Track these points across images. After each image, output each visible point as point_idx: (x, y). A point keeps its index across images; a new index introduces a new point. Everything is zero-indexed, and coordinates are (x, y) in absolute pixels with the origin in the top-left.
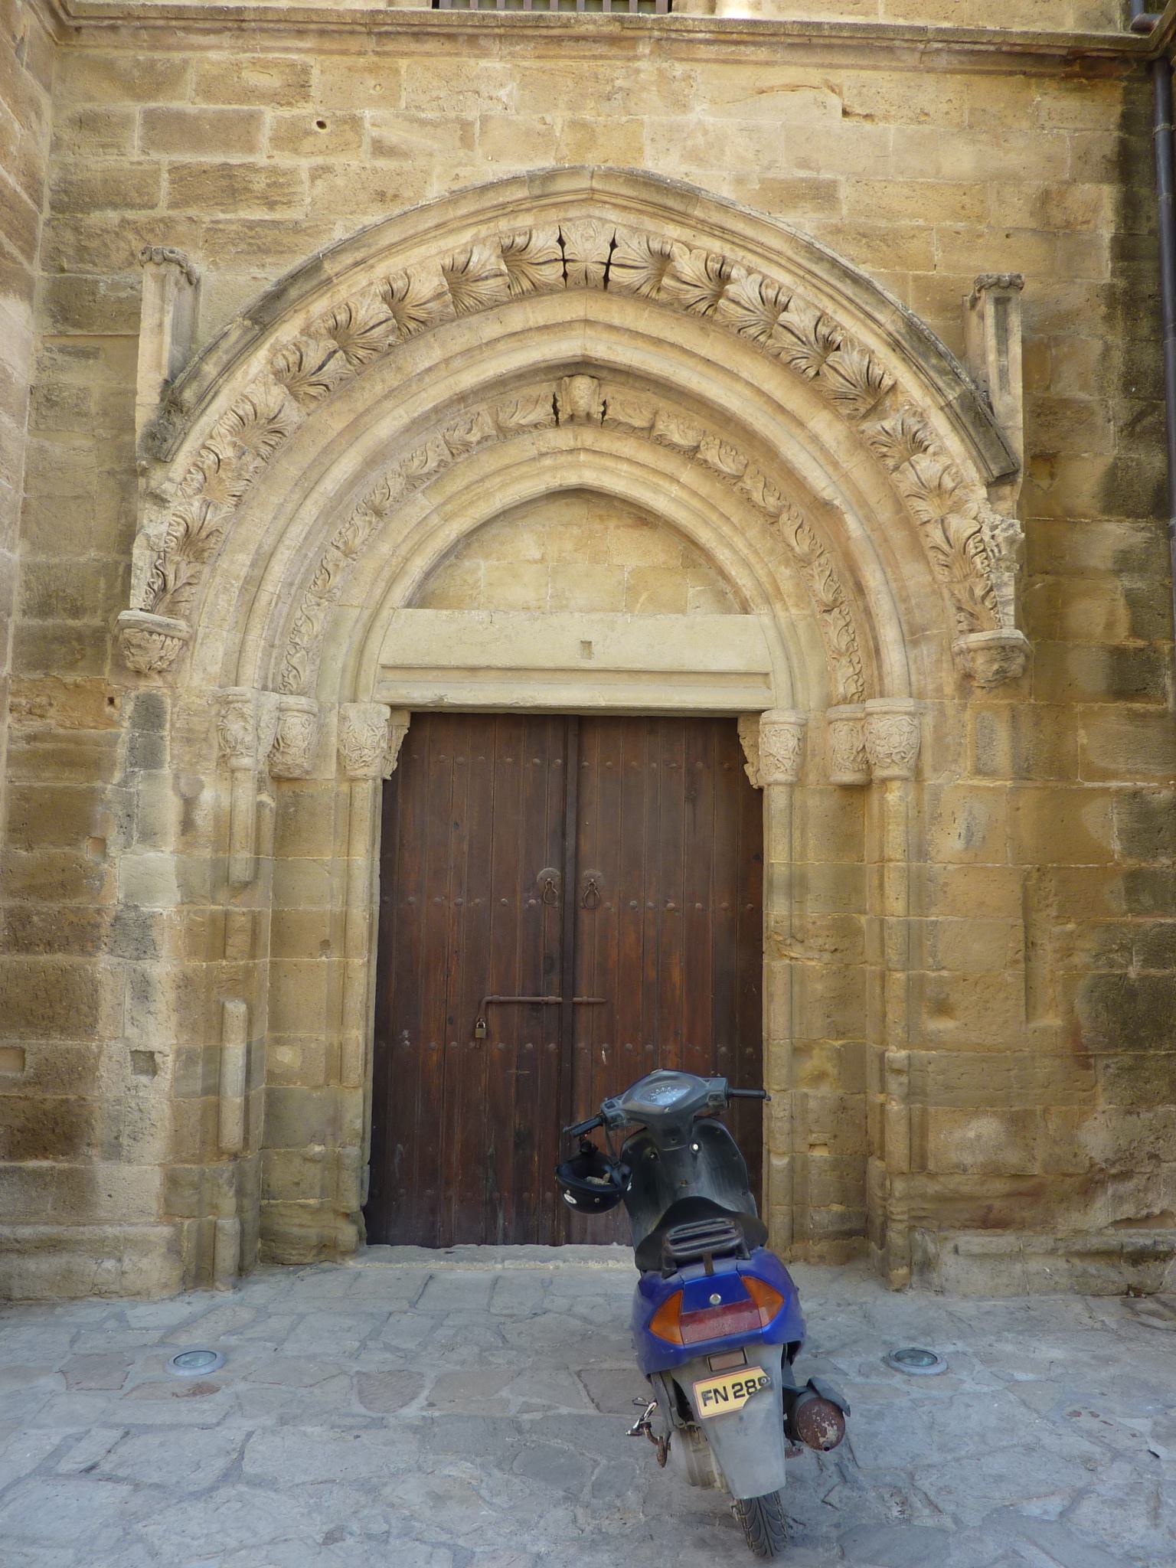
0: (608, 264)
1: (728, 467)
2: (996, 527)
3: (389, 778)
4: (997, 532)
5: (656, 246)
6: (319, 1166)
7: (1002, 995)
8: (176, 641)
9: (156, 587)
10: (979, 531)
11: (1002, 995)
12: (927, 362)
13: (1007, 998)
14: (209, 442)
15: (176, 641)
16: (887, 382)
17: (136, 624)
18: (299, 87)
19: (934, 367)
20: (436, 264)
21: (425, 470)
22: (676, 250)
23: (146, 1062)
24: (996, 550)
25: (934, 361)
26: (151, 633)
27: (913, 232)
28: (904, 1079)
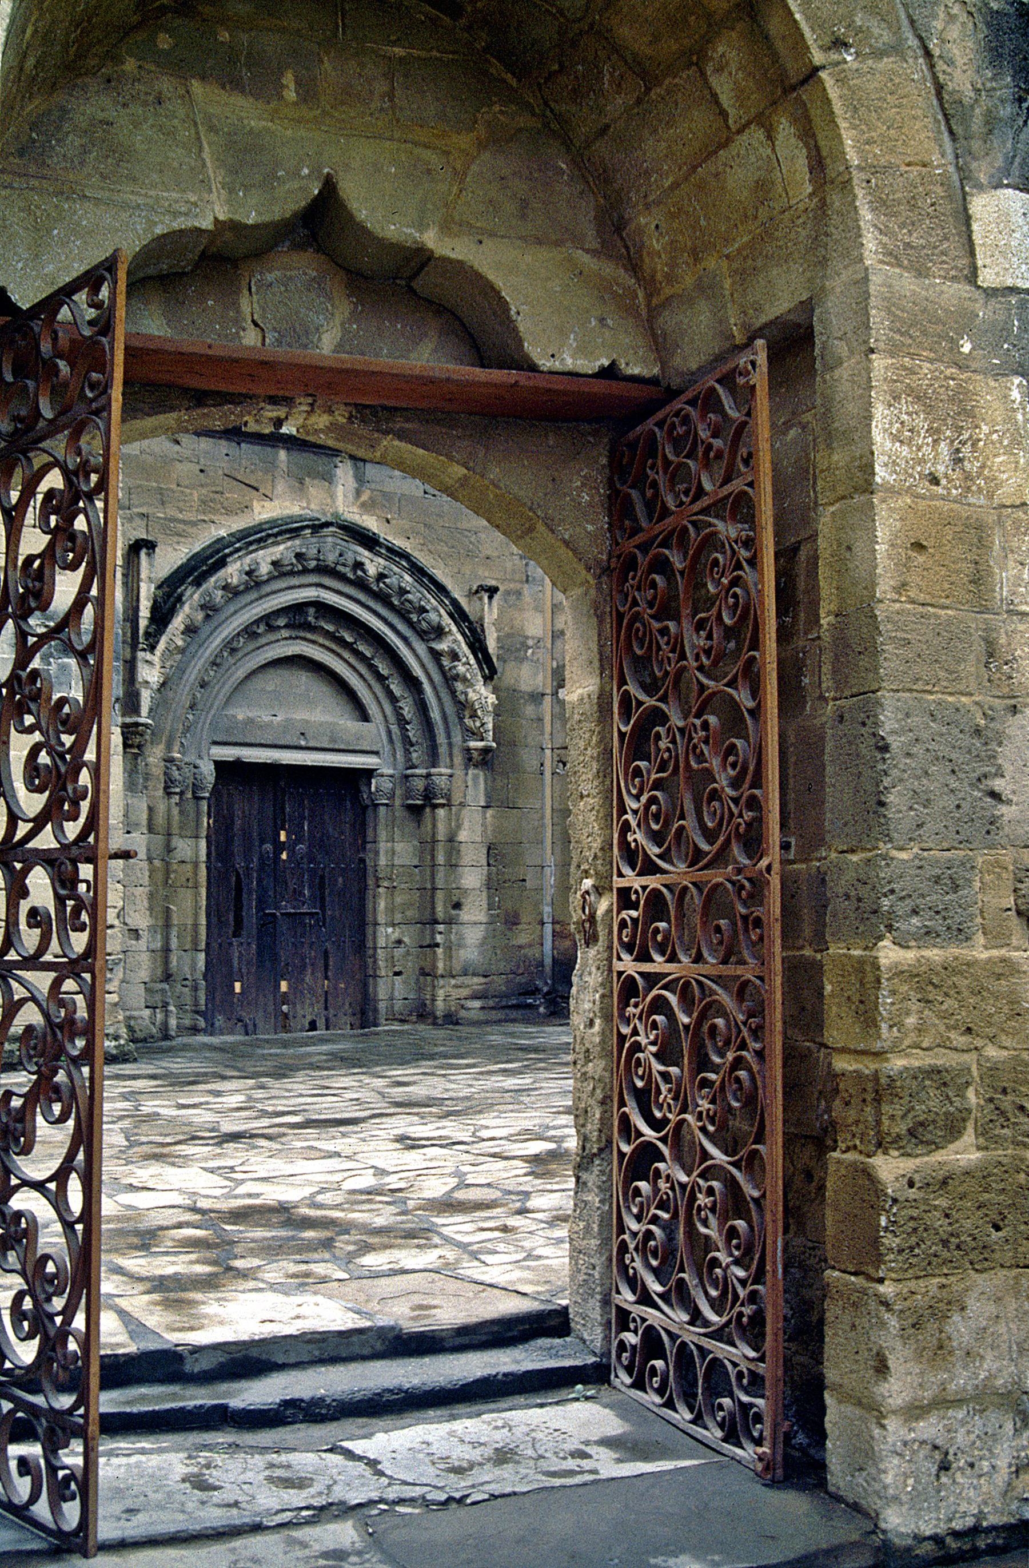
5: (358, 559)
20: (269, 560)
22: (367, 562)
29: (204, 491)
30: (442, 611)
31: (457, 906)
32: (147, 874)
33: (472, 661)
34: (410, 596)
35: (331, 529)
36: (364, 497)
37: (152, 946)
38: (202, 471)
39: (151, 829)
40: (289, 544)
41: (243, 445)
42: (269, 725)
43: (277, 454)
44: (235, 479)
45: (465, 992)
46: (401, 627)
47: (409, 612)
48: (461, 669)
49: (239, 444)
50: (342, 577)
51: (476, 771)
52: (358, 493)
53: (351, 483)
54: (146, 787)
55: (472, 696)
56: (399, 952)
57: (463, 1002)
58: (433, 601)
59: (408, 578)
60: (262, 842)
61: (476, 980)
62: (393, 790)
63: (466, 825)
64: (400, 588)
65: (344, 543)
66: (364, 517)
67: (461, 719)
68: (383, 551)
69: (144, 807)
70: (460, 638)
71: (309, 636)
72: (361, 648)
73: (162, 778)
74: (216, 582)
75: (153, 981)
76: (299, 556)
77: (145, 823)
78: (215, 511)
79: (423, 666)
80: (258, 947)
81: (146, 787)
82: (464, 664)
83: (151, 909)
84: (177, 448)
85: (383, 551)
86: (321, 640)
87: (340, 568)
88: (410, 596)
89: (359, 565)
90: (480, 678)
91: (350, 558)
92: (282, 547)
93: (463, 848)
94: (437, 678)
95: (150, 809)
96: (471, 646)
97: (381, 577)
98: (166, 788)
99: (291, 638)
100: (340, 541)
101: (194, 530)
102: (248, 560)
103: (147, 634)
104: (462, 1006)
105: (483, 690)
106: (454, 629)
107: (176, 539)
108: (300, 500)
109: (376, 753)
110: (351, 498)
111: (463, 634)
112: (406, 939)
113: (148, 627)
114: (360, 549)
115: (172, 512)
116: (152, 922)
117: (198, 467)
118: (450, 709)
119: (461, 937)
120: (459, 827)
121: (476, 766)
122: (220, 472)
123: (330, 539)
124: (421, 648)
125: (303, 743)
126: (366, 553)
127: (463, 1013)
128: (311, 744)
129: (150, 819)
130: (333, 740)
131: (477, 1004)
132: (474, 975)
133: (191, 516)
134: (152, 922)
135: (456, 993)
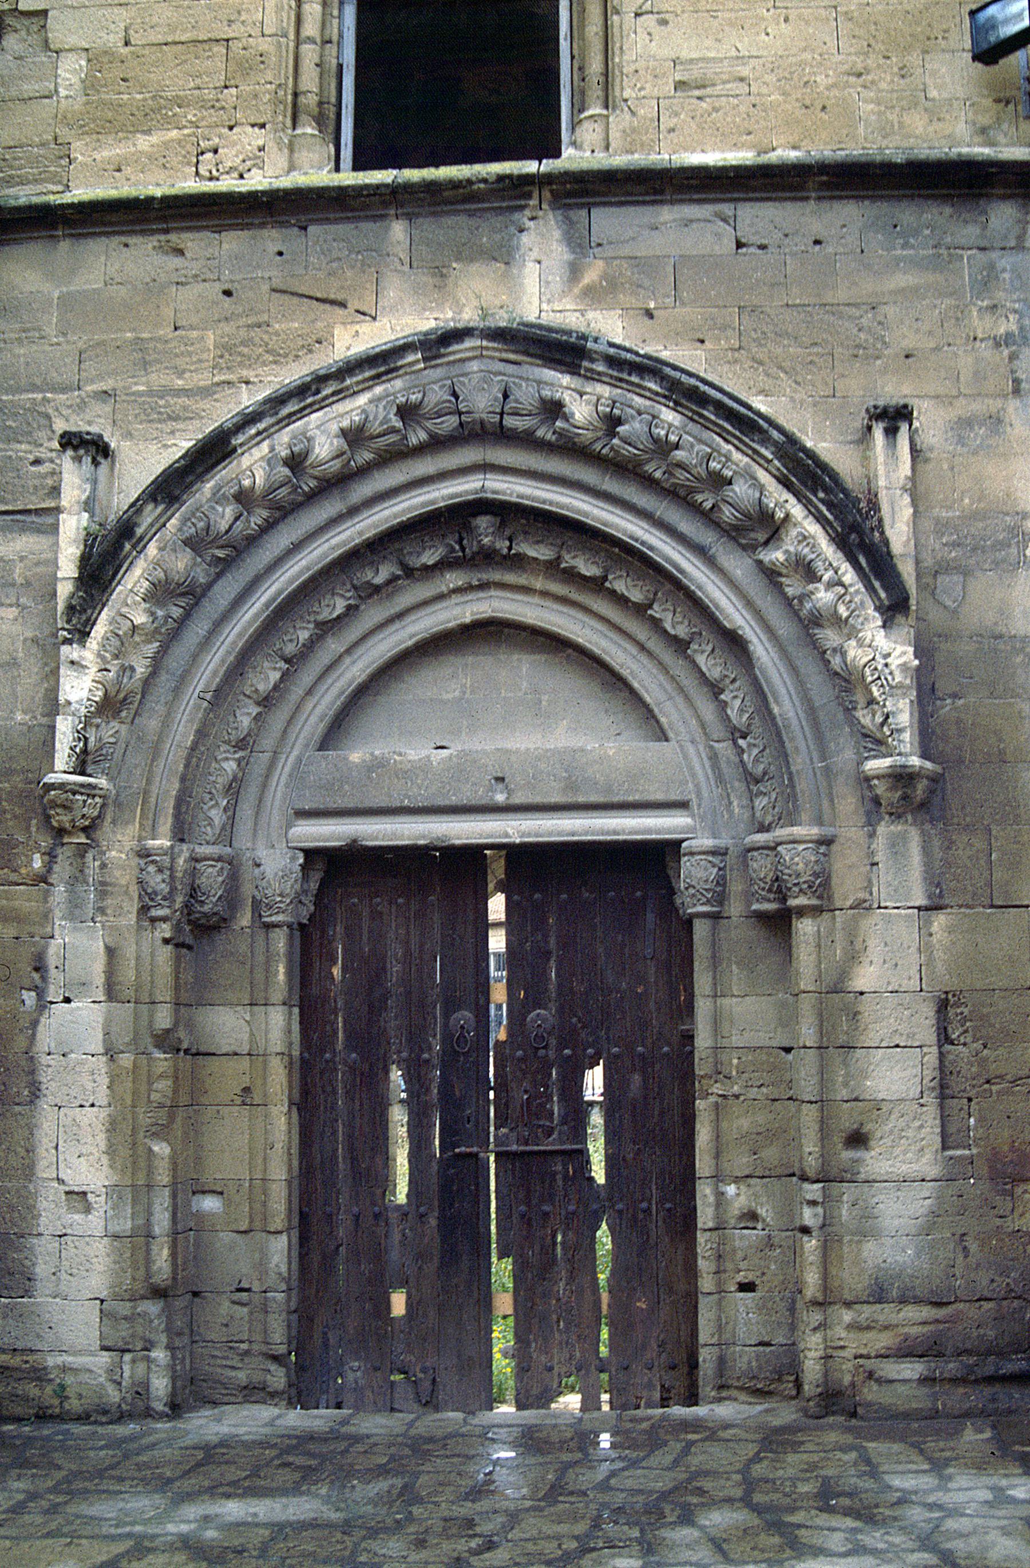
0: (502, 414)
1: (636, 596)
2: (889, 655)
3: (305, 921)
4: (889, 660)
5: (546, 393)
6: (246, 1310)
7: (917, 1124)
8: (97, 799)
9: (78, 750)
10: (873, 659)
11: (917, 1124)
12: (816, 496)
13: (921, 1127)
14: (124, 610)
15: (97, 799)
16: (780, 515)
17: (62, 786)
18: (210, 50)
19: (822, 501)
20: (334, 427)
21: (335, 615)
22: (567, 397)
23: (79, 1198)
24: (889, 678)
25: (821, 495)
26: (74, 794)
27: (809, 359)
28: (820, 1210)
29: (227, 328)
30: (763, 476)
31: (858, 1139)
32: (106, 1081)
33: (849, 576)
34: (679, 455)
35: (469, 343)
36: (591, 275)
37: (115, 1228)
38: (228, 293)
39: (112, 992)
40: (378, 390)
41: (311, 229)
42: (425, 767)
43: (387, 229)
44: (293, 294)
45: (883, 1341)
46: (687, 526)
47: (692, 490)
48: (823, 596)
49: (305, 229)
50: (527, 440)
51: (898, 828)
52: (574, 271)
53: (558, 252)
54: (102, 910)
55: (855, 654)
56: (745, 1239)
57: (869, 1364)
58: (736, 456)
59: (669, 415)
60: (451, 1006)
61: (912, 1312)
62: (721, 881)
63: (875, 950)
64: (656, 440)
65: (510, 369)
66: (591, 315)
67: (849, 711)
68: (600, 367)
69: (99, 947)
70: (813, 528)
71: (510, 578)
72: (620, 586)
73: (134, 890)
74: (218, 488)
75: (117, 1298)
76: (407, 412)
77: (99, 980)
78: (249, 361)
79: (749, 604)
80: (442, 1219)
81: (102, 910)
82: (830, 585)
83: (111, 1151)
84: (177, 261)
85: (600, 367)
86: (539, 584)
87: (510, 422)
88: (679, 455)
89: (554, 409)
90: (871, 611)
91: (525, 396)
92: (362, 400)
93: (866, 1006)
94: (785, 628)
95: (111, 952)
96: (841, 542)
97: (612, 422)
98: (144, 909)
99: (469, 588)
100: (501, 366)
101: (205, 404)
102: (284, 436)
103: (71, 609)
104: (870, 1375)
105: (881, 640)
106: (797, 511)
107: (171, 425)
108: (440, 306)
109: (682, 805)
110: (557, 280)
111: (820, 519)
112: (762, 1211)
113: (72, 596)
114: (549, 374)
115: (159, 378)
116: (114, 1179)
117: (219, 287)
118: (822, 692)
119: (867, 1215)
120: (854, 956)
121: (896, 816)
122: (265, 288)
123: (474, 366)
124: (738, 565)
125: (500, 798)
126: (566, 379)
127: (871, 1393)
128: (518, 799)
129: (110, 973)
130: (571, 786)
131: (911, 1370)
132: (903, 1301)
133: (203, 379)
134: (114, 1179)
135: (854, 1344)
